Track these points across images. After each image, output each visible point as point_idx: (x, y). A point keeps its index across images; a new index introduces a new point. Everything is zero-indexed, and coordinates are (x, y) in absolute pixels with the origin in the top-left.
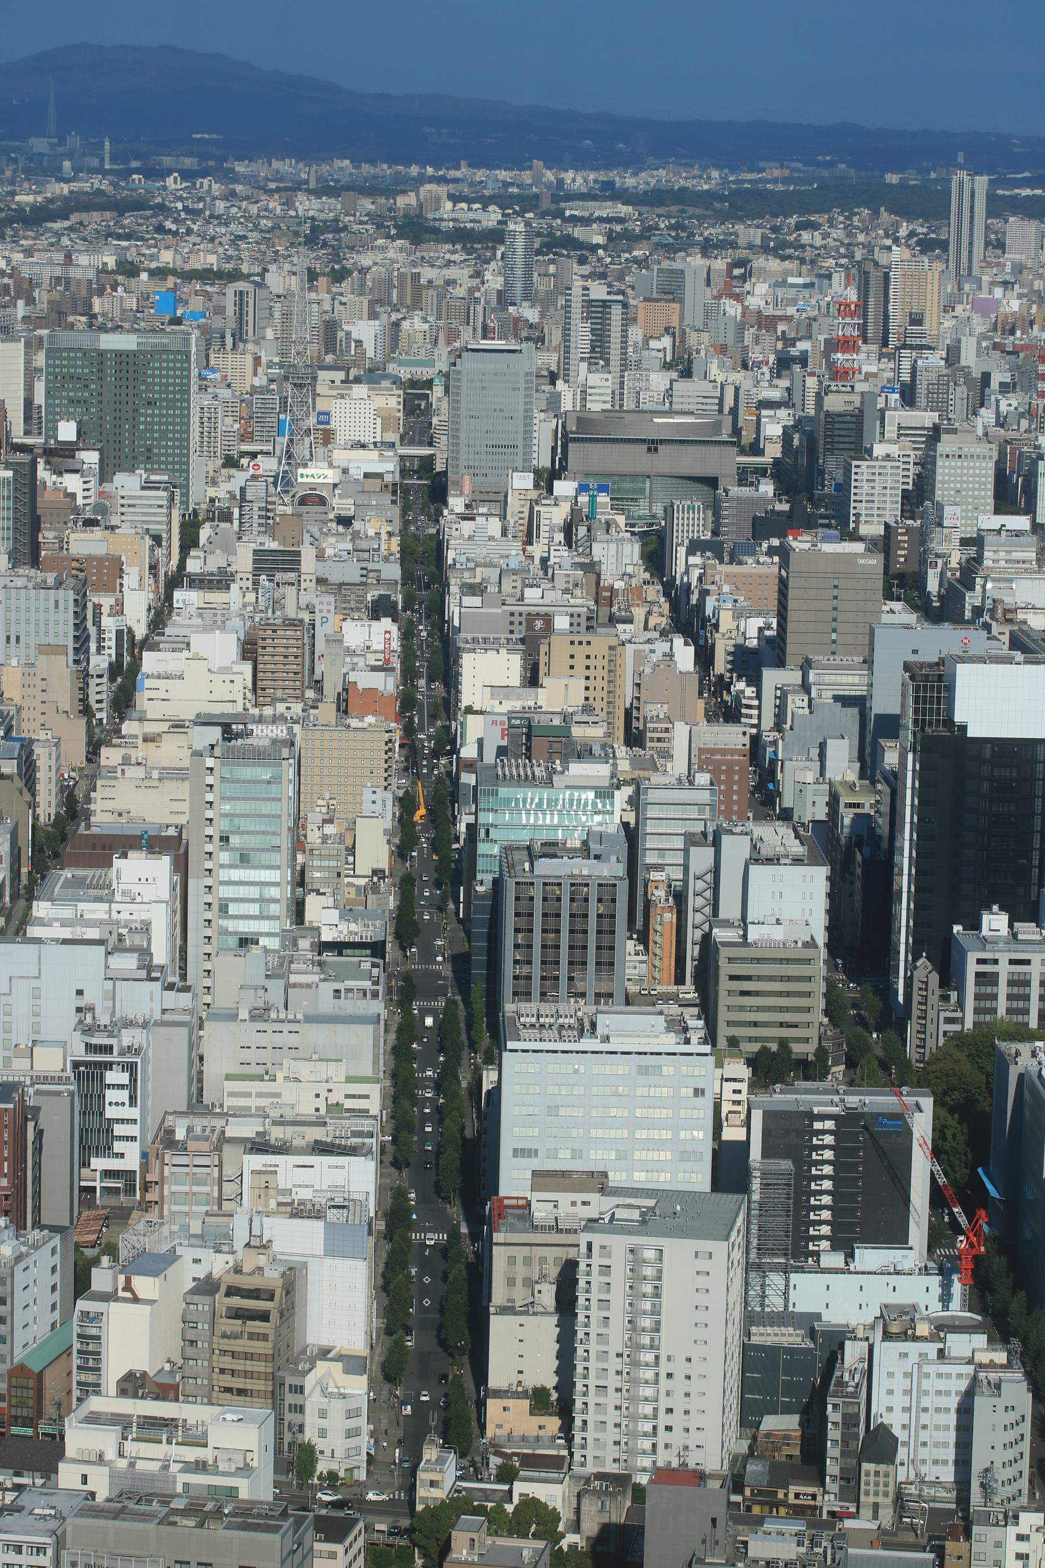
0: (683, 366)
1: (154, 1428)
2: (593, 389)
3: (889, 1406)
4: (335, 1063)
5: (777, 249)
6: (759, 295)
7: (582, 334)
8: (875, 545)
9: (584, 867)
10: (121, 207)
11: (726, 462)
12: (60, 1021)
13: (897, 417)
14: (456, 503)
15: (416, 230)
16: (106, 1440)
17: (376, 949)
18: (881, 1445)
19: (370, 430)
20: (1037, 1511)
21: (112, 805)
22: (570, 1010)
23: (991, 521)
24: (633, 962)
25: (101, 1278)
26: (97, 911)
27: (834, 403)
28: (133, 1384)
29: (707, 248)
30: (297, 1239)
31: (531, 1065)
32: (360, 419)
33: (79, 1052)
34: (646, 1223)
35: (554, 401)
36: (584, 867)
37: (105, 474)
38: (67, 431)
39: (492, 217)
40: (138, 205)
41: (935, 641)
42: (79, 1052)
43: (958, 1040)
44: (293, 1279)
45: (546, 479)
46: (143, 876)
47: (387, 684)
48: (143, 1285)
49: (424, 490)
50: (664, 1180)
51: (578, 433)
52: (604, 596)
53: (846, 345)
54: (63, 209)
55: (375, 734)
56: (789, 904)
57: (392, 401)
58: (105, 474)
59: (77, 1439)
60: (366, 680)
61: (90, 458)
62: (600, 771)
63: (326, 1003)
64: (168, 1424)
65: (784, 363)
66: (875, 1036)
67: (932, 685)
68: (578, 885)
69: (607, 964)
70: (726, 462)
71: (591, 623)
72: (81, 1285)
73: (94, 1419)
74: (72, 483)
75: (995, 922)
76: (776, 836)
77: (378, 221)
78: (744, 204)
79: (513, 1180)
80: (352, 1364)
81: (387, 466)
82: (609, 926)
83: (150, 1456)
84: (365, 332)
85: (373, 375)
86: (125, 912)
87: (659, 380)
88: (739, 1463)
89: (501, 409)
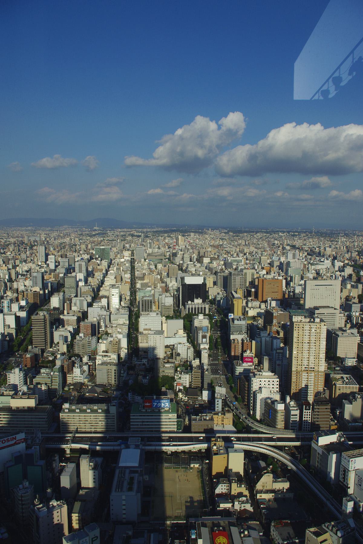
0: (159, 248)
1: (105, 356)
2: (150, 251)
3: (179, 351)
4: (123, 320)
5: (169, 236)
6: (167, 241)
7: (149, 245)
8: (178, 265)
9: (148, 298)
10: (103, 234)
11: (163, 258)
12: (96, 315)
13: (180, 253)
14: (136, 263)
15: (133, 235)
16: (101, 357)
17: (128, 307)
18: (179, 355)
19: (128, 255)
20: (202, 393)
21: (101, 293)
22: (147, 313)
23: (189, 263)
24: (154, 308)
25: (100, 341)
26: (100, 304)
27: (174, 251)
28: (103, 352)
29: (162, 237)
30: (120, 336)
31: (143, 318)
32: (127, 254)
33: (98, 318)
34: (155, 334)
35: (146, 252)
36: (148, 298)
37: (101, 260)
38: (97, 256)
39: (140, 234)
40: (105, 234)
41: (183, 275)
42: (98, 318)
43: (186, 314)
44: (120, 340)
45: (145, 260)
46: (104, 302)
47: (129, 280)
48: (105, 342)
49: (132, 262)
50: (157, 329)
51: (149, 255)
52: (151, 271)
53: (175, 246)
54: (97, 234)
55: (128, 286)
56: (169, 301)
57: (130, 252)
58: (101, 260)
59: (98, 357)
60: (127, 280)
61: (100, 259)
62: (150, 289)
63: (123, 313)
64: (107, 356)
65: (169, 248)
66: (215, 480)
67: (183, 279)
68: (148, 300)
69: (151, 308)
70: (163, 258)
71: (150, 274)
72: (98, 342)
73: (100, 355)
74: (98, 261)
75: (190, 302)
76: (168, 294)
77: (129, 235)
78: (165, 232)
79: (141, 329)
80: (125, 349)
81: (130, 259)
82: (148, 306)
83: (105, 359)
84: (127, 246)
85: (128, 250)
86: (102, 304)
87: (157, 250)
88: (165, 357)
89: (140, 251)
